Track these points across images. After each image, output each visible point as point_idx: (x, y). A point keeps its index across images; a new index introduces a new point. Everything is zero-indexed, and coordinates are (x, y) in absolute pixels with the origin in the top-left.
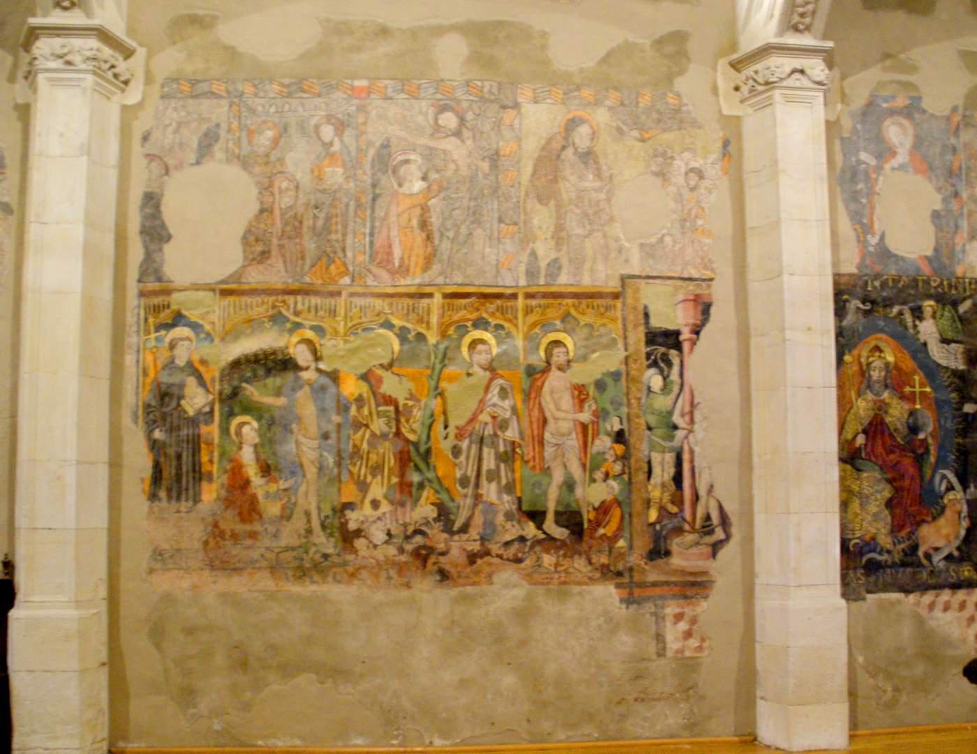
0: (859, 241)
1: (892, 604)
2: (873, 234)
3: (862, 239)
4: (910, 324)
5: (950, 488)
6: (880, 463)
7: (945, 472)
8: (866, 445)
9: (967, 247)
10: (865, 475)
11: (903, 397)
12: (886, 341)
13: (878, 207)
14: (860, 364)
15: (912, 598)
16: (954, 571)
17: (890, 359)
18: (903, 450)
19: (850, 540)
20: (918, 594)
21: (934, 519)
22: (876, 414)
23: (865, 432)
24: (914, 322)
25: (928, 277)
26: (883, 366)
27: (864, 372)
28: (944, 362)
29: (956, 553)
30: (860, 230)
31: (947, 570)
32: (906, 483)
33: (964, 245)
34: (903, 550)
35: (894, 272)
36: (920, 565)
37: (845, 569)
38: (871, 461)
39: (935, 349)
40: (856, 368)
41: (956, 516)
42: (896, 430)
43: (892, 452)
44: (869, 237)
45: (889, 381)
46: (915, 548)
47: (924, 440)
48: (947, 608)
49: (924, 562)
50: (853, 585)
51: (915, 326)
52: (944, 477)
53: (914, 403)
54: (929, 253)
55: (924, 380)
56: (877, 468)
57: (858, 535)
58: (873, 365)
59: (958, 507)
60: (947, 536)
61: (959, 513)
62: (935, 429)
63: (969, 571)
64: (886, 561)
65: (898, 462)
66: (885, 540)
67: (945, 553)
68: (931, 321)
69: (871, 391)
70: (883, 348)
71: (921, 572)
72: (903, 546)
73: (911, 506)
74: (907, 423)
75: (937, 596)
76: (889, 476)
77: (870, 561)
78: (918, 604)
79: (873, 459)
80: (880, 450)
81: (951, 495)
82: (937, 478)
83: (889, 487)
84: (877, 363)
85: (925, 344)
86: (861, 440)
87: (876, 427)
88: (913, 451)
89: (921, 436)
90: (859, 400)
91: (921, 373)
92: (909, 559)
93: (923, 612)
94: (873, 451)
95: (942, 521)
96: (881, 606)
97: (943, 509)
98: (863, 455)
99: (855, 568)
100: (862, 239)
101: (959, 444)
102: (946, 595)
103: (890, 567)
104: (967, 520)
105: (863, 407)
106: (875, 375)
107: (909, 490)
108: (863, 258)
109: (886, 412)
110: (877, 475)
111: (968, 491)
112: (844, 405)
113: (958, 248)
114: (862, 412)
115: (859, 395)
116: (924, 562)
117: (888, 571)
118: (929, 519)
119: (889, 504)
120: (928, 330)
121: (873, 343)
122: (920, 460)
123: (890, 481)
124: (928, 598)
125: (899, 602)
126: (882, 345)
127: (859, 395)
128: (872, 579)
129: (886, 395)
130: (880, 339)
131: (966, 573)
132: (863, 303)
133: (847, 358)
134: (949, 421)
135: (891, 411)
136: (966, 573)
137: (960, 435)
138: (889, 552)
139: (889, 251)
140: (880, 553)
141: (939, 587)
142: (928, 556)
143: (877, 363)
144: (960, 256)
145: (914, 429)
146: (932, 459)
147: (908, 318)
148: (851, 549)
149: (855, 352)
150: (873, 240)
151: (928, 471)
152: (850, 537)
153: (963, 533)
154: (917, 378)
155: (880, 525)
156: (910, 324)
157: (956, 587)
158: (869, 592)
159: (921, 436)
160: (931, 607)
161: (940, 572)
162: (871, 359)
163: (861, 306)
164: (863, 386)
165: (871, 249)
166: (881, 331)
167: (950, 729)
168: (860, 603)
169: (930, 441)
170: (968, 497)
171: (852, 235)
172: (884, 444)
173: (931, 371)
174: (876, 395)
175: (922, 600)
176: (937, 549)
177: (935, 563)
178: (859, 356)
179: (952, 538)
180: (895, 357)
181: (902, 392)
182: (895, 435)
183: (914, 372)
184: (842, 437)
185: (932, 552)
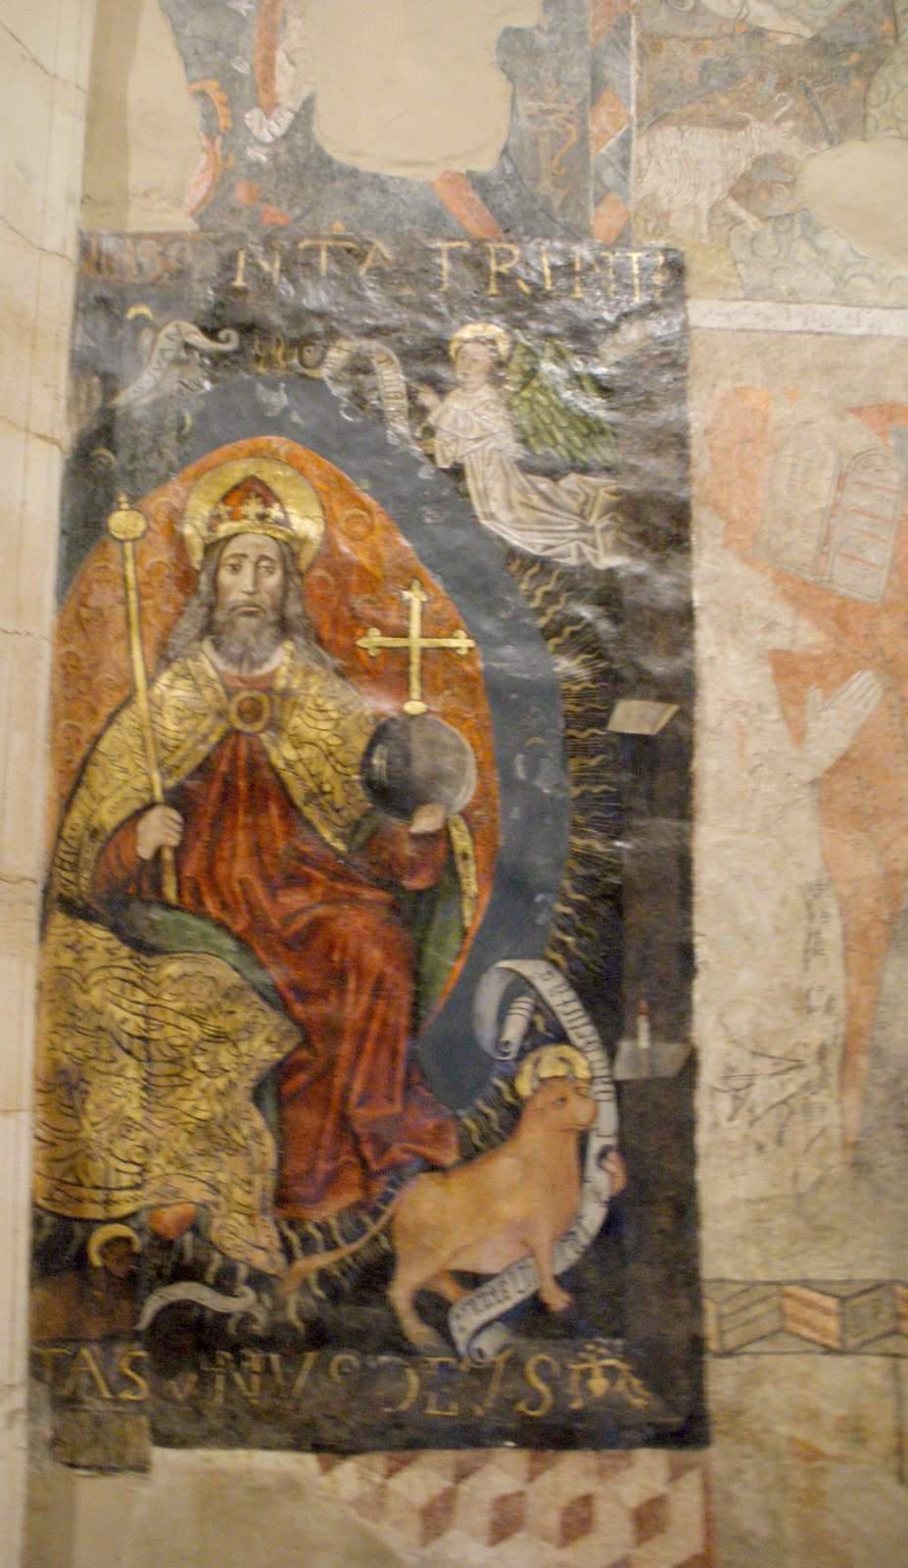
0: (210, 133)
1: (261, 1493)
2: (270, 109)
3: (223, 122)
4: (396, 406)
5: (548, 1033)
6: (239, 926)
7: (530, 969)
8: (179, 851)
9: (638, 148)
10: (173, 968)
11: (354, 668)
12: (290, 461)
13: (294, 23)
14: (179, 544)
15: (350, 1477)
16: (543, 1368)
17: (307, 525)
18: (341, 875)
19: (91, 1224)
20: (379, 1461)
21: (470, 1154)
22: (233, 733)
23: (180, 799)
24: (411, 395)
25: (478, 243)
26: (271, 551)
27: (192, 576)
28: (528, 541)
29: (558, 1300)
30: (217, 97)
31: (515, 1364)
32: (353, 1008)
33: (625, 142)
34: (324, 1277)
35: (339, 227)
36: (397, 1343)
37: (51, 1362)
38: (203, 916)
39: (497, 489)
40: (161, 555)
41: (571, 1148)
42: (316, 795)
43: (296, 880)
44: (253, 118)
45: (294, 609)
46: (377, 1273)
47: (443, 835)
48: (505, 1524)
49: (495, 461)
50: (95, 1405)
51: (418, 412)
52: (520, 986)
53: (402, 690)
54: (485, 164)
55: (448, 609)
56: (229, 944)
57: (127, 1209)
58: (234, 548)
59: (580, 1111)
60: (521, 1230)
61: (583, 1140)
62: (483, 793)
63: (611, 1373)
64: (247, 1318)
65: (317, 925)
66: (247, 1237)
67: (514, 1293)
68: (486, 393)
69: (217, 646)
70: (278, 488)
71: (399, 1373)
72: (323, 1260)
73: (365, 1100)
74: (365, 764)
75: (462, 1475)
76: (276, 974)
77: (177, 1311)
78: (376, 1503)
79: (211, 905)
80: (240, 868)
81: (549, 1062)
82: (489, 993)
83: (271, 1021)
84: (252, 540)
85: (457, 472)
86: (159, 831)
87: (229, 787)
88: (390, 884)
89: (425, 822)
90: (164, 679)
91: (437, 582)
92: (347, 1316)
93: (399, 1536)
94: (210, 872)
95: (503, 1167)
96: (211, 1495)
97: (514, 1112)
98: (170, 892)
99: (110, 1339)
100: (223, 122)
101: (587, 858)
102: (503, 1472)
103: (267, 1343)
104: (613, 1163)
105: (175, 705)
106: (238, 586)
107: (362, 1035)
108: (222, 182)
109: (276, 726)
110: (223, 971)
111: (625, 1046)
112: (83, 699)
113: (604, 150)
114: (170, 724)
115: (163, 657)
116: (417, 1331)
117: (254, 1359)
118: (449, 1157)
119: (276, 1088)
120: (473, 424)
121: (238, 471)
122: (416, 911)
123: (277, 1000)
124: (423, 1478)
125: (291, 1486)
126: (274, 475)
127: (163, 657)
128: (182, 1387)
129: (281, 661)
130: (273, 456)
131: (599, 1385)
132: (211, 333)
133: (123, 521)
134: (548, 766)
135: (296, 721)
136: (599, 1385)
137: (599, 824)
138: (259, 1280)
139: (329, 161)
140: (224, 1283)
141: (470, 1436)
142: (433, 1307)
143: (252, 540)
144: (609, 177)
145: (393, 794)
146: (471, 915)
147: (391, 379)
148: (96, 1260)
149: (160, 500)
150: (266, 128)
151: (448, 964)
152: (94, 1212)
153: (594, 1216)
154: (415, 598)
155: (228, 1170)
156: (396, 406)
157: (552, 1435)
158: (164, 1440)
159: (425, 822)
160: (436, 1517)
161: (482, 1373)
162: (225, 528)
163: (199, 340)
164: (188, 626)
165: (261, 156)
166: (277, 424)
167: (416, 1005)
168: (125, 1481)
169: (462, 841)
170: (622, 1072)
171: (191, 114)
172: (257, 850)
173: (481, 576)
174: (238, 661)
175: (399, 1484)
176: (472, 1281)
177: (460, 1339)
178: (176, 516)
179: (543, 1237)
180: (329, 520)
181: (353, 652)
182: (310, 812)
183: (408, 577)
184: (76, 817)
185: (448, 1289)
